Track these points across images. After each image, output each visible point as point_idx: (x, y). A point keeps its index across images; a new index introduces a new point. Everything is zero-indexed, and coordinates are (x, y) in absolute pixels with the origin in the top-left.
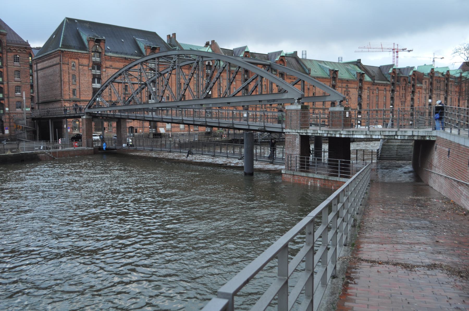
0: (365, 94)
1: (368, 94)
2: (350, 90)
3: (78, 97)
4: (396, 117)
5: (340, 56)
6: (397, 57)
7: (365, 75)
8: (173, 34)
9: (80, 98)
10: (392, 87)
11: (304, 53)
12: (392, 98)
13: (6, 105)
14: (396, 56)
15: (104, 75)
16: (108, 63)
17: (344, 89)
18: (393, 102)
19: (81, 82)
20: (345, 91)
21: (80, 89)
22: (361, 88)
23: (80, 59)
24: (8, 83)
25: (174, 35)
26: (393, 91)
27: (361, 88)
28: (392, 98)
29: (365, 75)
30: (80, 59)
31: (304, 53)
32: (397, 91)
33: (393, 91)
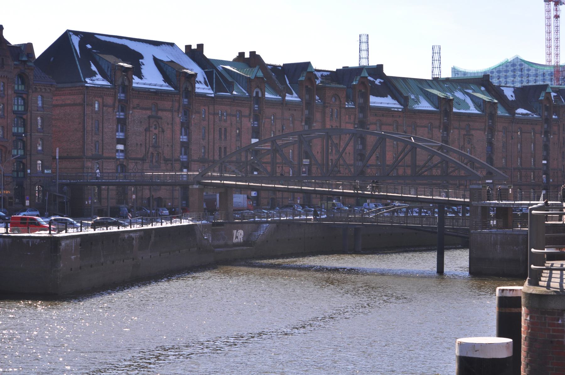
0: (499, 138)
1: (504, 140)
2: (473, 132)
3: (101, 153)
4: (553, 181)
5: (436, 44)
6: (557, 17)
7: (499, 105)
8: (198, 45)
9: (103, 153)
10: (546, 126)
11: (364, 39)
12: (546, 147)
13: (29, 166)
14: (553, 13)
15: (130, 120)
16: (135, 102)
17: (463, 132)
18: (548, 154)
19: (105, 130)
20: (464, 135)
21: (103, 141)
22: (491, 130)
23: (105, 97)
24: (31, 135)
25: (200, 46)
26: (546, 133)
27: (491, 130)
28: (546, 147)
29: (499, 105)
30: (105, 97)
31: (364, 39)
32: (554, 134)
33: (546, 133)
